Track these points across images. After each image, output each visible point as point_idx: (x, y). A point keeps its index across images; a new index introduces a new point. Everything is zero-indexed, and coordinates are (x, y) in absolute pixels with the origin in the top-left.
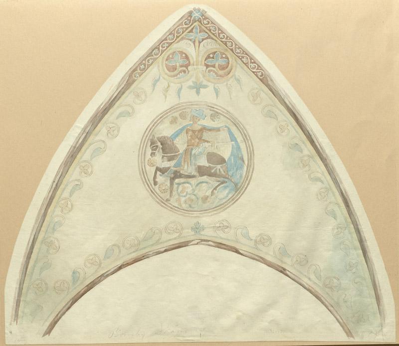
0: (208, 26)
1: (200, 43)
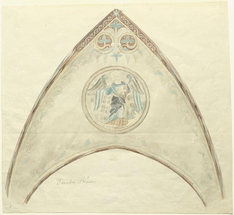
0: (86, 41)
1: (118, 30)
